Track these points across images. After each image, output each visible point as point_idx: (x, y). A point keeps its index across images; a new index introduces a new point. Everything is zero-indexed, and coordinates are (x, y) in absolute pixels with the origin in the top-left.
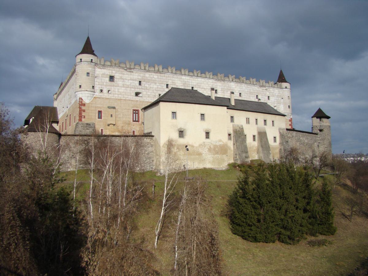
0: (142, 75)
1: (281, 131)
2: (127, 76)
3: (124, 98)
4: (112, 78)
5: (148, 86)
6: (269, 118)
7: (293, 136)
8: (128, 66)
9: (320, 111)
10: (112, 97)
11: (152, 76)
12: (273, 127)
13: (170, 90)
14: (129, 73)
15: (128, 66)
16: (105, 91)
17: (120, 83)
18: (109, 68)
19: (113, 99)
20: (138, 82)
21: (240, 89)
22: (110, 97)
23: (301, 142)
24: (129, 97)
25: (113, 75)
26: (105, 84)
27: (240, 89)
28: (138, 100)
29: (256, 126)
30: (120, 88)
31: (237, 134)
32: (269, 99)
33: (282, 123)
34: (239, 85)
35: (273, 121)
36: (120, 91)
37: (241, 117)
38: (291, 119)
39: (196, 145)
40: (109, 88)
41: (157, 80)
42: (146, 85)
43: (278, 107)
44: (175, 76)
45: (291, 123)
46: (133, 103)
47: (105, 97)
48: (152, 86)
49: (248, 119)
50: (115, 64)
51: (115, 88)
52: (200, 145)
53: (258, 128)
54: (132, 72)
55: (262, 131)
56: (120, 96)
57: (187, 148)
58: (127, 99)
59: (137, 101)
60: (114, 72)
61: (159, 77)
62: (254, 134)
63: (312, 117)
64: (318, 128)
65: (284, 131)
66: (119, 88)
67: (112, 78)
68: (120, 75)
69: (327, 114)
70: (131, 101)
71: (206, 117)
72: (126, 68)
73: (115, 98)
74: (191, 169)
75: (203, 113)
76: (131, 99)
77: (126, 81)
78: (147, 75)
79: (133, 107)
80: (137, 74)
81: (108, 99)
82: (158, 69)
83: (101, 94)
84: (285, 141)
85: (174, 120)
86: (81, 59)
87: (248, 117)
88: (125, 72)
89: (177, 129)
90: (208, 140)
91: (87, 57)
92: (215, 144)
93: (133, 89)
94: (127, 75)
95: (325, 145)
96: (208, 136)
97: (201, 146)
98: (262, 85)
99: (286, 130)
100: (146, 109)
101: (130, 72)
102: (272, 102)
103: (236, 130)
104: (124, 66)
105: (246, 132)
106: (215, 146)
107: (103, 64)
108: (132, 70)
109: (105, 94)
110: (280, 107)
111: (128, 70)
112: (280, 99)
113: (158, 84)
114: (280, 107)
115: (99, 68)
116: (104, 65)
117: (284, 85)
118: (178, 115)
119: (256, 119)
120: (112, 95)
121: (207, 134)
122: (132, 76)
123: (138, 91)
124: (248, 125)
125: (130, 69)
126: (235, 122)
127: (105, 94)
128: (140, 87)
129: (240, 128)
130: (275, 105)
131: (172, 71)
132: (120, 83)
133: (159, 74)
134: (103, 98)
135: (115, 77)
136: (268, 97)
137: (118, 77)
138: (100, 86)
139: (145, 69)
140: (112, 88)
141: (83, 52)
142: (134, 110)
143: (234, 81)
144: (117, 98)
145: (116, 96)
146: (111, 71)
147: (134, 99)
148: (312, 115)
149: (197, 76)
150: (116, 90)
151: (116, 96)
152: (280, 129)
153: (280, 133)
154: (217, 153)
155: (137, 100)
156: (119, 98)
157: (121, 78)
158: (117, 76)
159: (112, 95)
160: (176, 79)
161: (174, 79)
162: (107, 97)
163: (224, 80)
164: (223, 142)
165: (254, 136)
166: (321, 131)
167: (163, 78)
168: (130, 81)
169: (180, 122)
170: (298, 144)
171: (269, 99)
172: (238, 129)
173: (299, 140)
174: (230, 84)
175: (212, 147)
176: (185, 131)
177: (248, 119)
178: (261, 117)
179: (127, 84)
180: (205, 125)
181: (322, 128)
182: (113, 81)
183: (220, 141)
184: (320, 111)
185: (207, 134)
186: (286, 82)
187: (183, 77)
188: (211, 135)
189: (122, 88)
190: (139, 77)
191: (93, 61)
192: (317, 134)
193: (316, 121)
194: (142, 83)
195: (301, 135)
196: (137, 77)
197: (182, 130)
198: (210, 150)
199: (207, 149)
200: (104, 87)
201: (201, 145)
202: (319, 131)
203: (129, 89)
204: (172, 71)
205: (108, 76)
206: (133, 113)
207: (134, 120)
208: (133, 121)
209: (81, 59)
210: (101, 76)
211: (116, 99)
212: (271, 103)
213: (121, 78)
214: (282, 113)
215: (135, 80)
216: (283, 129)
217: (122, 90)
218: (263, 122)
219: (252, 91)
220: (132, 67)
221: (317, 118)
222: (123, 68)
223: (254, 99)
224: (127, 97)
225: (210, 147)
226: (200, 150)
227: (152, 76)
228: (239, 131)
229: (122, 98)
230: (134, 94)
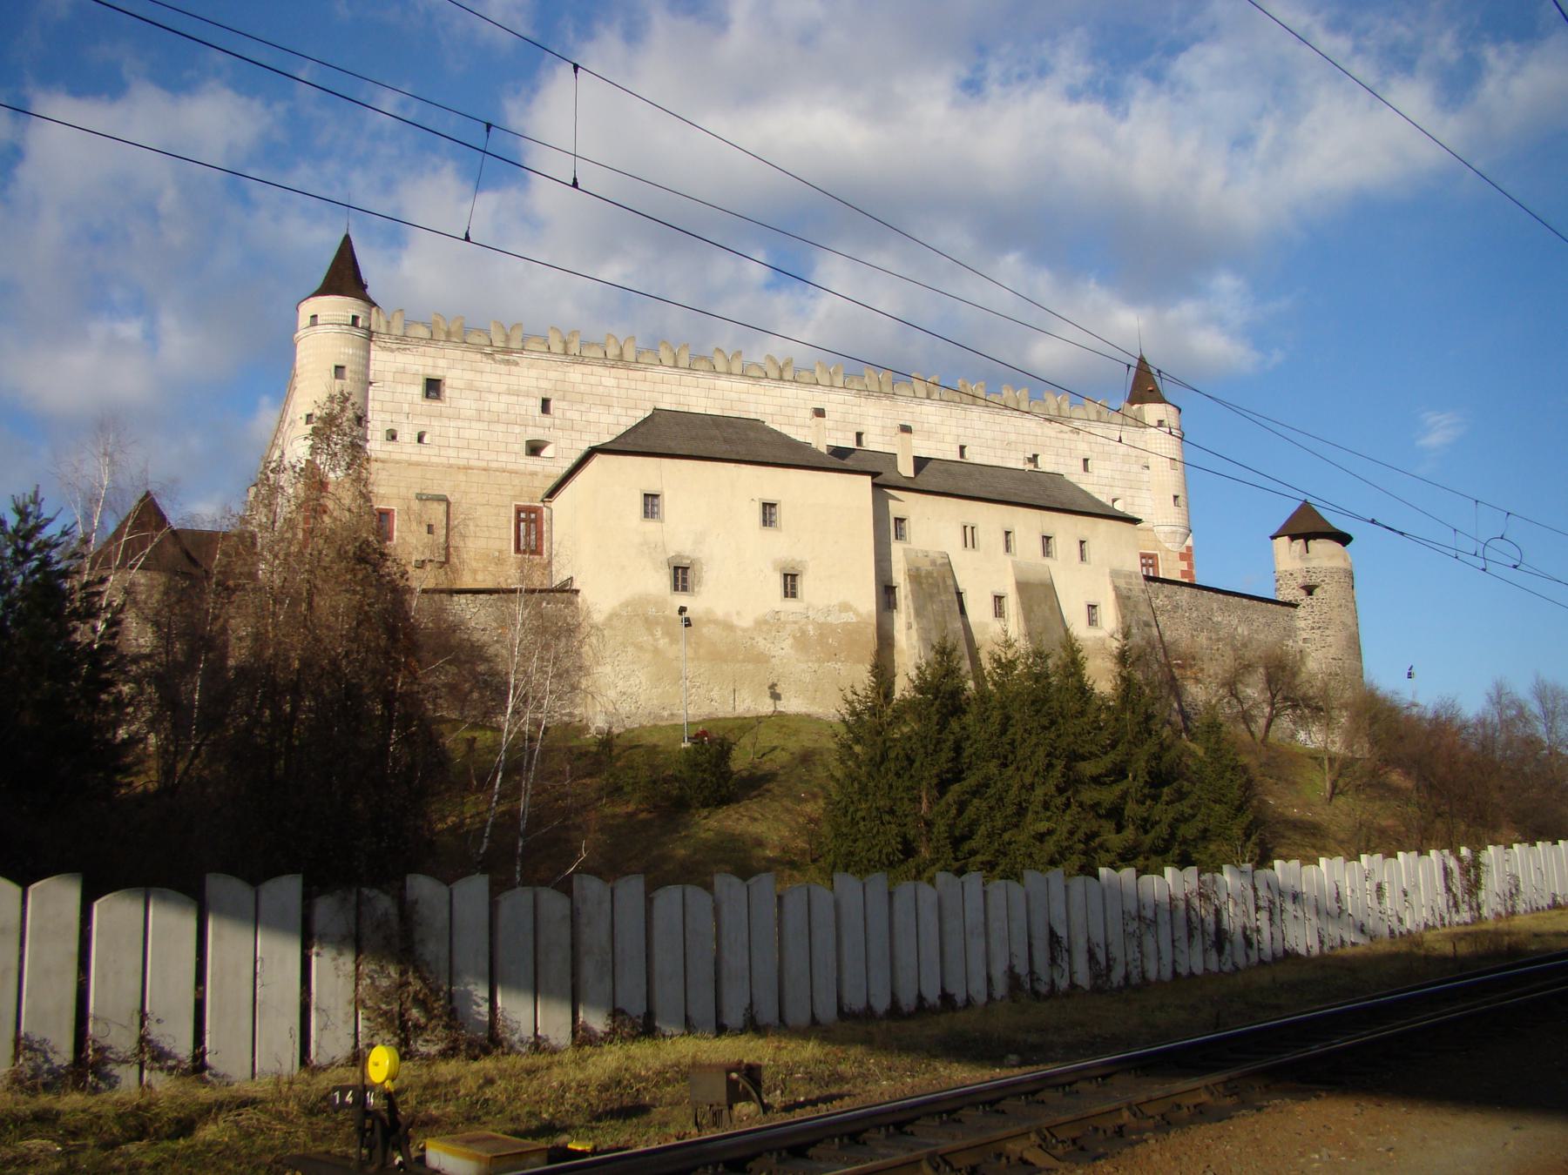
0: (552, 375)
1: (1122, 583)
2: (493, 378)
3: (484, 464)
4: (433, 387)
5: (576, 416)
6: (1066, 528)
7: (1176, 607)
8: (499, 343)
9: (1306, 510)
10: (434, 460)
11: (593, 379)
12: (1084, 566)
13: (645, 421)
14: (503, 368)
15: (499, 343)
16: (407, 435)
17: (467, 404)
18: (421, 349)
19: (437, 465)
20: (540, 403)
21: (961, 431)
22: (425, 459)
23: (1217, 633)
24: (503, 457)
25: (436, 374)
26: (406, 408)
27: (961, 431)
28: (539, 469)
29: (1008, 559)
30: (466, 424)
31: (920, 584)
32: (1086, 469)
33: (1114, 551)
34: (957, 412)
35: (1082, 542)
36: (467, 434)
37: (932, 525)
38: (1189, 548)
39: (746, 622)
40: (421, 423)
41: (615, 392)
42: (569, 414)
43: (1129, 500)
44: (688, 379)
45: (1190, 566)
46: (516, 482)
47: (404, 457)
48: (592, 417)
49: (968, 530)
50: (448, 334)
51: (446, 422)
52: (761, 623)
53: (1015, 566)
54: (517, 364)
55: (1033, 577)
56: (465, 454)
57: (687, 614)
58: (494, 465)
59: (534, 474)
60: (442, 363)
61: (625, 383)
62: (999, 591)
63: (1273, 537)
64: (1300, 580)
65: (1134, 581)
66: (460, 424)
67: (433, 387)
68: (469, 375)
69: (1339, 523)
70: (511, 472)
71: (783, 514)
72: (488, 350)
73: (445, 461)
74: (721, 715)
75: (770, 498)
76: (510, 466)
77: (492, 397)
78: (576, 374)
79: (514, 497)
80: (533, 373)
81: (418, 464)
82: (617, 352)
83: (391, 446)
84: (1138, 623)
85: (651, 526)
86: (315, 317)
87: (970, 521)
88: (487, 365)
89: (663, 558)
90: (791, 604)
91: (336, 307)
92: (822, 620)
93: (517, 429)
94: (492, 374)
95: (1332, 650)
96: (794, 587)
97: (765, 628)
98: (1053, 412)
99: (1142, 581)
100: (552, 493)
101: (508, 362)
102: (1104, 481)
103: (918, 569)
104: (484, 340)
105: (964, 581)
106: (825, 630)
107: (400, 333)
108: (514, 357)
109: (407, 447)
110: (1137, 501)
111: (498, 357)
112: (1136, 468)
113: (618, 411)
114: (1137, 501)
115: (383, 349)
116: (403, 338)
117: (1153, 412)
118: (668, 505)
119: (1007, 533)
120: (436, 451)
121: (790, 583)
122: (513, 380)
123: (535, 434)
124: (970, 554)
125: (507, 351)
126: (913, 539)
127: (407, 447)
128: (547, 420)
129: (933, 563)
130: (1116, 492)
131: (676, 361)
132: (467, 404)
133: (622, 373)
134: (398, 462)
135: (448, 382)
136: (1086, 460)
137: (460, 383)
138: (387, 417)
139: (566, 353)
140: (435, 423)
141: (327, 289)
142: (519, 510)
143: (936, 396)
144: (452, 461)
145: (452, 453)
146: (430, 361)
147: (522, 467)
148: (1274, 530)
149: (781, 379)
150: (452, 432)
151: (452, 453)
152: (1115, 574)
153: (1116, 588)
154: (834, 656)
155: (531, 468)
156: (462, 463)
157: (470, 387)
158: (453, 379)
159: (436, 451)
160: (693, 392)
161: (682, 390)
162: (415, 458)
163: (892, 395)
164: (856, 613)
165: (998, 599)
166: (1309, 590)
167: (640, 385)
168: (504, 398)
169: (679, 530)
170: (1202, 639)
171: (1086, 469)
172: (926, 566)
173: (1206, 623)
174: (918, 409)
175: (811, 630)
176: (697, 567)
177: (968, 530)
178: (1027, 524)
179: (495, 407)
180: (781, 546)
181: (1314, 581)
182: (438, 397)
183: (845, 607)
184: (1306, 510)
185: (790, 583)
186: (1162, 400)
187: (723, 383)
188: (805, 585)
189: (474, 424)
190: (544, 384)
191: (360, 323)
192: (1295, 606)
193: (1287, 554)
194: (553, 404)
195: (1215, 606)
196: (534, 383)
197: (686, 562)
198: (802, 642)
199: (790, 641)
200: (403, 418)
201: (766, 622)
202: (1301, 595)
203: (501, 427)
204: (676, 361)
205: (421, 381)
206: (518, 521)
207: (522, 547)
208: (518, 550)
209: (315, 317)
210: (389, 377)
211: (451, 466)
212: (1098, 485)
213: (470, 387)
214: (1105, 499)
215: (528, 395)
216: (1129, 575)
217: (473, 431)
218: (1037, 545)
219: (1013, 437)
220: (514, 345)
221: (1293, 537)
222: (479, 349)
223: (1016, 461)
224: (493, 456)
225: (803, 632)
226: (762, 644)
227: (593, 379)
228: (929, 574)
229: (473, 463)
230: (521, 448)
